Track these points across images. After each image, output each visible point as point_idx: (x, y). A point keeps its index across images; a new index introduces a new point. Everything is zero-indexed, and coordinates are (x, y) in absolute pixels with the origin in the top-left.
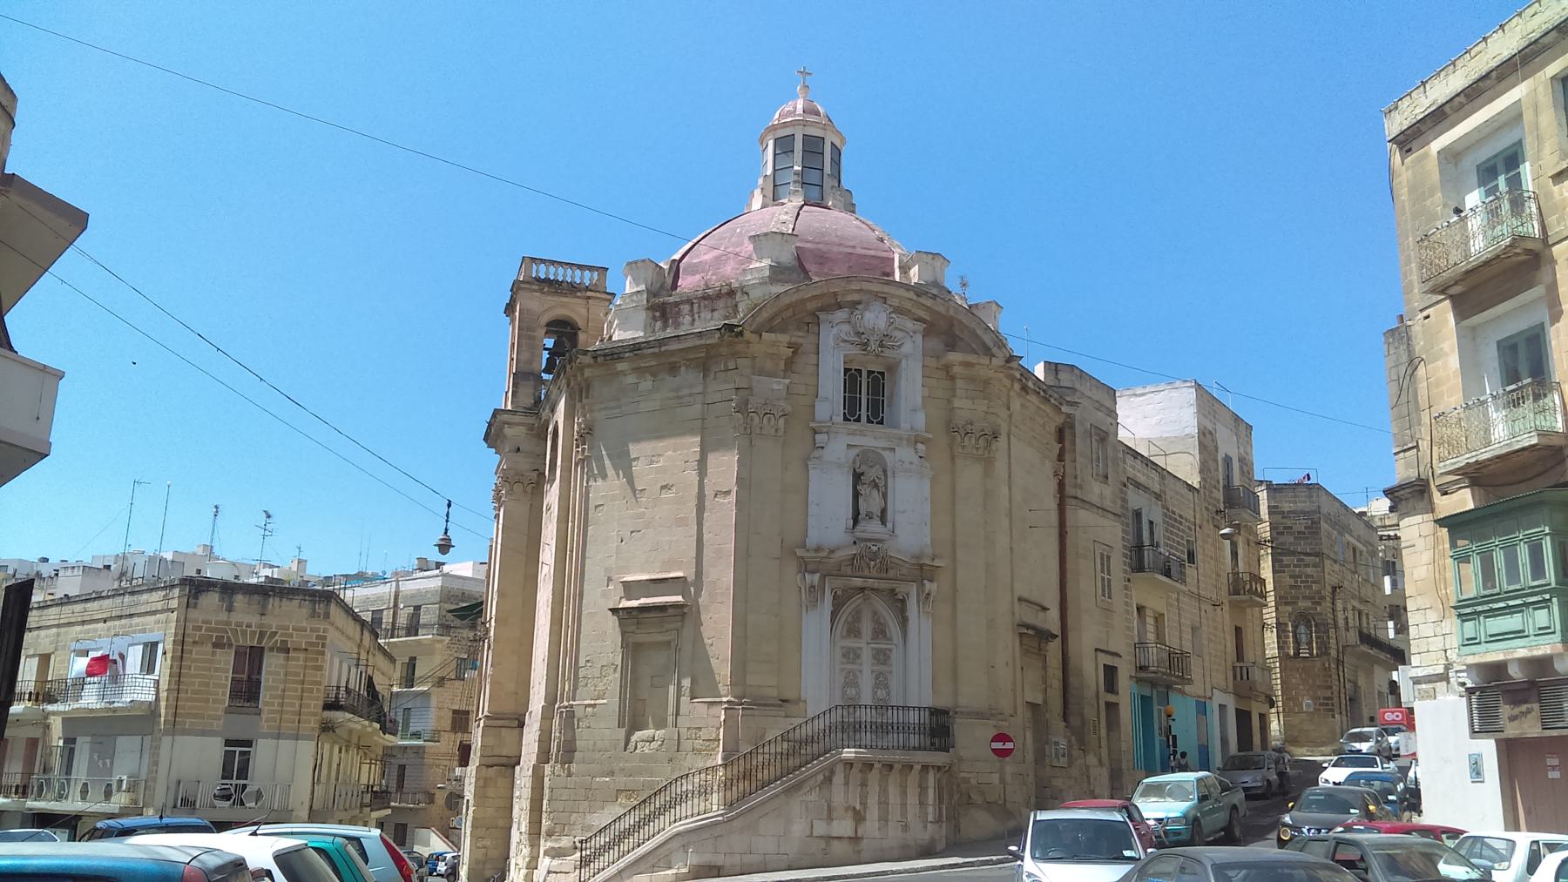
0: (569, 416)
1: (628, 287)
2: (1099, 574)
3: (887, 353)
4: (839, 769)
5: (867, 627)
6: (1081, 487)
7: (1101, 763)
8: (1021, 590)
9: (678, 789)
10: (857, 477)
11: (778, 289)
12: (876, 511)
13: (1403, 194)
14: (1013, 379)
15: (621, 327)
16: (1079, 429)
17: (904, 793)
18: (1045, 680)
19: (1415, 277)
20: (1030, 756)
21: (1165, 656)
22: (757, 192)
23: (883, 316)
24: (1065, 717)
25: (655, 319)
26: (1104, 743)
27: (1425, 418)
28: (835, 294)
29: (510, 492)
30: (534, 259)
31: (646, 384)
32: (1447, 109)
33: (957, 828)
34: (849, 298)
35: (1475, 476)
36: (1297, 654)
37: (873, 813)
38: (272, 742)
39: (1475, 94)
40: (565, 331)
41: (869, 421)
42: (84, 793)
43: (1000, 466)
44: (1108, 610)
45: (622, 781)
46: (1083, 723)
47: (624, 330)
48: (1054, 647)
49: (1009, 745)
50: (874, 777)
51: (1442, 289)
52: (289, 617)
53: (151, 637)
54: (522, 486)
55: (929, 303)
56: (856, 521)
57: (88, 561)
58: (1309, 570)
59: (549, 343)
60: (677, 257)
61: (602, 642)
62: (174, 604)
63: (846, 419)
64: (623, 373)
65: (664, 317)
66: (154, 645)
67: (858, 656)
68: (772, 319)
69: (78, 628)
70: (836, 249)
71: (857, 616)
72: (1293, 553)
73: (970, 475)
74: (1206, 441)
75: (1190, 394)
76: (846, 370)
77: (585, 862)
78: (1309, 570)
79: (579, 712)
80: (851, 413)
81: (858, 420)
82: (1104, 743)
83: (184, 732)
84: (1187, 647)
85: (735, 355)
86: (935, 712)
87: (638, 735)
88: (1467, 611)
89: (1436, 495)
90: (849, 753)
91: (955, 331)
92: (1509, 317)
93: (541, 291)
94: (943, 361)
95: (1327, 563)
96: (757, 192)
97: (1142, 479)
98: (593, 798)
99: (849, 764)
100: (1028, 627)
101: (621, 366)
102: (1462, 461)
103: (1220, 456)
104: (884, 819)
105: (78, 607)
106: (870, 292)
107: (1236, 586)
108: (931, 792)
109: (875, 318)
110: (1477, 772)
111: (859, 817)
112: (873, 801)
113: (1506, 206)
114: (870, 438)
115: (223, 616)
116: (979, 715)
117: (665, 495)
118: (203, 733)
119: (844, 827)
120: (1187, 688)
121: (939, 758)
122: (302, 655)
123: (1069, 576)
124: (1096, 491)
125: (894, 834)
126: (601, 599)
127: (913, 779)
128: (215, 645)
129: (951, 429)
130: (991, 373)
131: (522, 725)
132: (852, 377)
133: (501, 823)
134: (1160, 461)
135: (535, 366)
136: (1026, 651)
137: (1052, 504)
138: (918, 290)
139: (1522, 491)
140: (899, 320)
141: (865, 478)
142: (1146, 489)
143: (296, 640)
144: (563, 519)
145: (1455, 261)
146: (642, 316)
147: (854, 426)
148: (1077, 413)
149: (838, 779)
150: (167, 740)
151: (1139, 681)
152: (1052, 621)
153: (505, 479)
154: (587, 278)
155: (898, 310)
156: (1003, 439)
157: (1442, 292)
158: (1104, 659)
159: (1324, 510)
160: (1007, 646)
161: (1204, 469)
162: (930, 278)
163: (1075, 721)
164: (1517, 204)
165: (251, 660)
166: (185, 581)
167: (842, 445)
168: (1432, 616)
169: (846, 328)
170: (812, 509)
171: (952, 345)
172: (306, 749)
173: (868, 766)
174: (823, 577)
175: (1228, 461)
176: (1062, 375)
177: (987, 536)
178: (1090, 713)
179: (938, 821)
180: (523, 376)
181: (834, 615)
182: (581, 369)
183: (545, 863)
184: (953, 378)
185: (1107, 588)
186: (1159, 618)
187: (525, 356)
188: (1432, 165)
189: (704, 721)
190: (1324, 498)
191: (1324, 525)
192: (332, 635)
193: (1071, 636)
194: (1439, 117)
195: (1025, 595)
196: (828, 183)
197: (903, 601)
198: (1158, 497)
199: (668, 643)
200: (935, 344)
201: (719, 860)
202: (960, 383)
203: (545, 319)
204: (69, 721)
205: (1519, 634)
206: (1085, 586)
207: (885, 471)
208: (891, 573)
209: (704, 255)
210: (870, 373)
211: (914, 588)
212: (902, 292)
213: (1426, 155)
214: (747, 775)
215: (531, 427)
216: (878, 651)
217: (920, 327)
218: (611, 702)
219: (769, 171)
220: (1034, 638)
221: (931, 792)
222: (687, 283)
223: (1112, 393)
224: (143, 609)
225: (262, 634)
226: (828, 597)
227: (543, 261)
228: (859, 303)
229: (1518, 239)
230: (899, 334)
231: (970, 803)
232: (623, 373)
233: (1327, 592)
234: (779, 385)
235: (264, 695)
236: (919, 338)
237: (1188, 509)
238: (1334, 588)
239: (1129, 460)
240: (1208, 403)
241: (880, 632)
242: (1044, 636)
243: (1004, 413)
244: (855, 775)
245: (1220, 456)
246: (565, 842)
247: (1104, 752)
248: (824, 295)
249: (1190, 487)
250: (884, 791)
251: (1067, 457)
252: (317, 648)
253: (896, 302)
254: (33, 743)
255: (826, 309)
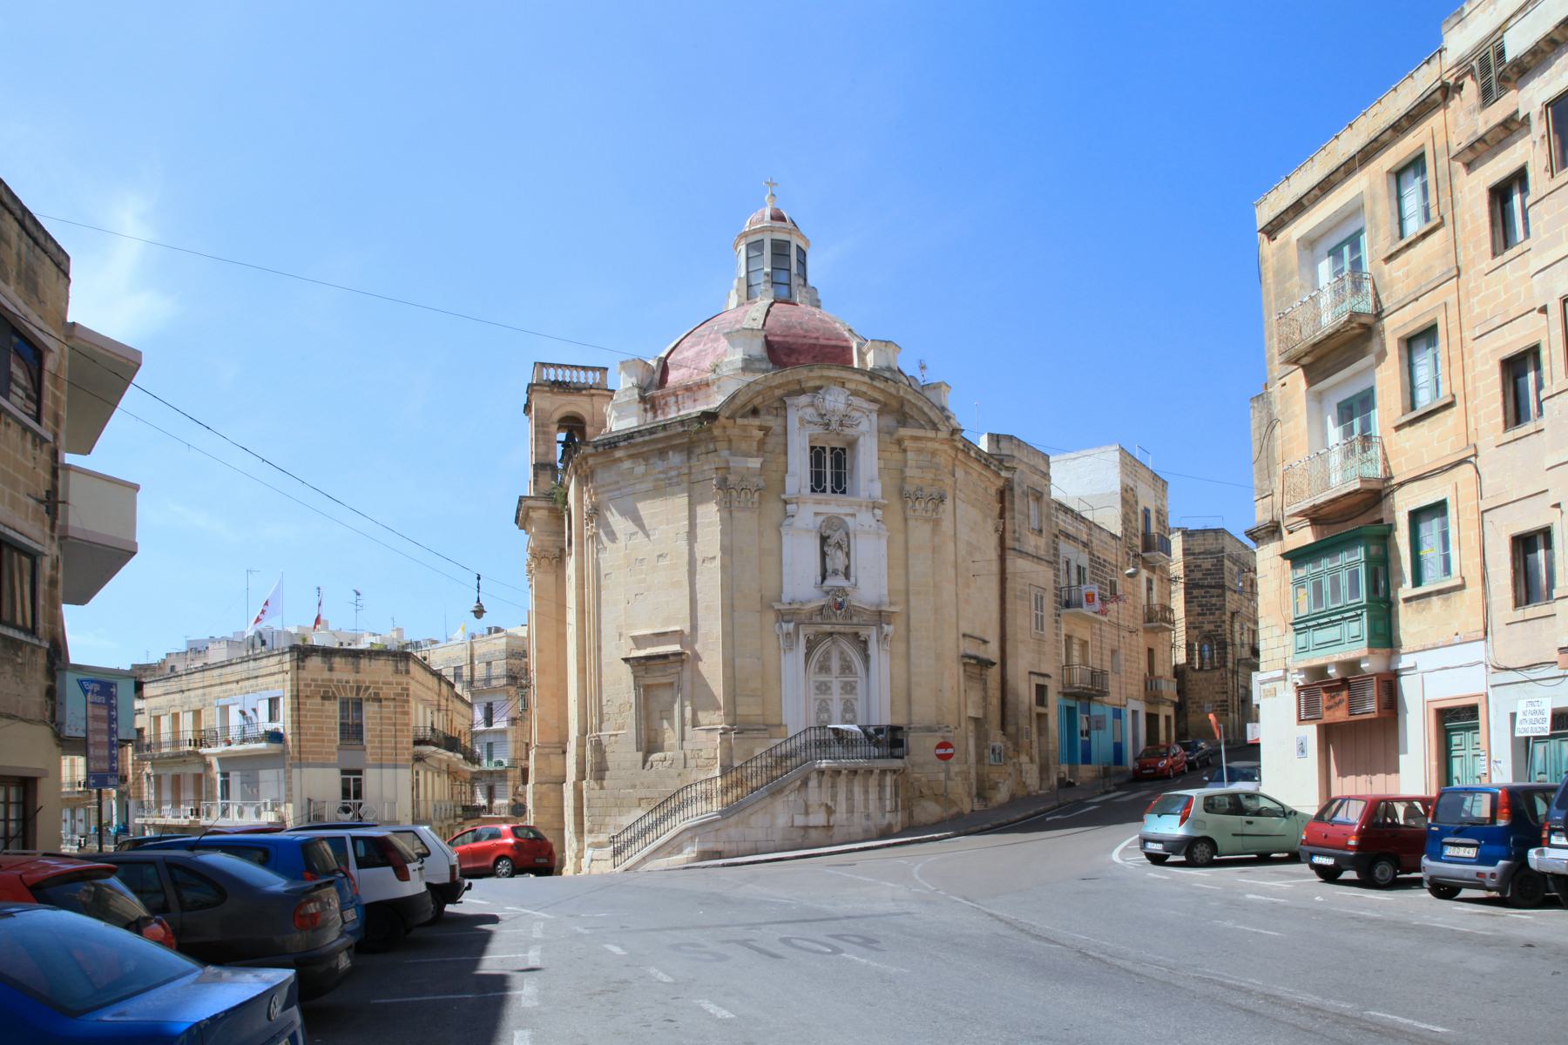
0: (579, 499)
1: (623, 383)
2: (1034, 612)
3: (847, 431)
4: (814, 776)
5: (835, 664)
6: (1018, 540)
7: (1032, 761)
8: (965, 627)
9: (683, 796)
10: (824, 540)
11: (750, 378)
12: (841, 568)
13: (1269, 277)
14: (957, 449)
15: (618, 419)
16: (1017, 491)
17: (866, 792)
18: (985, 698)
19: (1275, 351)
20: (972, 758)
21: (1088, 675)
22: (733, 293)
23: (842, 399)
24: (1003, 726)
25: (645, 410)
26: (1035, 744)
27: (1280, 470)
28: (799, 382)
29: (539, 565)
30: (543, 365)
31: (640, 469)
32: (1305, 201)
33: (911, 815)
34: (811, 384)
35: (1316, 516)
36: (1201, 668)
37: (842, 807)
38: (377, 771)
39: (1326, 186)
40: (574, 426)
41: (833, 491)
42: (241, 813)
43: (947, 525)
44: (1040, 641)
45: (643, 793)
46: (1018, 730)
47: (620, 419)
48: (993, 674)
49: (950, 751)
50: (842, 781)
51: (1294, 360)
52: (378, 673)
53: (273, 694)
54: (550, 558)
55: (881, 385)
56: (824, 578)
57: (230, 635)
58: (1214, 600)
59: (562, 436)
60: (663, 355)
61: (620, 685)
62: (287, 666)
63: (813, 490)
64: (620, 460)
65: (654, 409)
66: (277, 699)
67: (829, 688)
68: (744, 406)
69: (218, 689)
70: (800, 341)
71: (827, 655)
72: (1202, 587)
73: (920, 533)
74: (1128, 497)
75: (1116, 456)
76: (812, 448)
77: (617, 852)
78: (1214, 600)
79: (605, 741)
80: (817, 484)
81: (824, 491)
82: (1035, 744)
83: (309, 765)
84: (1107, 666)
85: (714, 439)
86: (894, 729)
87: (655, 757)
88: (1301, 625)
89: (1285, 532)
90: (824, 764)
91: (906, 407)
92: (1344, 384)
93: (552, 391)
94: (896, 436)
95: (1228, 594)
96: (733, 293)
97: (1071, 530)
98: (621, 805)
99: (821, 772)
100: (970, 657)
101: (619, 454)
102: (1306, 504)
103: (1140, 509)
104: (851, 811)
105: (216, 672)
106: (828, 378)
107: (1150, 616)
108: (888, 790)
109: (835, 400)
110: (1302, 750)
111: (830, 811)
112: (842, 797)
113: (1348, 285)
114: (833, 505)
115: (326, 675)
116: (929, 729)
117: (663, 563)
118: (324, 766)
119: (818, 818)
120: (1106, 699)
121: (897, 764)
122: (392, 704)
123: (1008, 615)
124: (1032, 543)
125: (859, 823)
126: (616, 651)
127: (873, 781)
128: (324, 698)
129: (903, 495)
130: (937, 445)
131: (564, 752)
132: (817, 454)
133: (556, 825)
134: (1088, 515)
135: (551, 457)
136: (969, 677)
137: (993, 554)
138: (873, 375)
139: (1350, 526)
140: (856, 401)
141: (830, 541)
142: (1075, 539)
143: (386, 692)
144: (581, 586)
145: (1309, 335)
146: (637, 408)
147: (819, 496)
148: (1016, 478)
149: (813, 783)
150: (296, 771)
151: (1065, 695)
152: (992, 652)
153: (534, 556)
154: (591, 378)
155: (855, 393)
156: (948, 502)
157: (1295, 363)
158: (1036, 680)
159: (1227, 551)
160: (953, 674)
161: (1126, 520)
162: (884, 364)
163: (1011, 729)
164: (1357, 286)
165: (353, 705)
166: (293, 648)
167: (810, 512)
168: (1277, 632)
169: (810, 410)
170: (786, 569)
171: (903, 419)
172: (405, 775)
173: (838, 772)
174: (797, 625)
175: (1146, 511)
176: (1002, 444)
177: (931, 589)
178: (1024, 723)
179: (894, 810)
180: (541, 467)
181: (808, 656)
182: (585, 458)
183: (588, 853)
184: (905, 451)
185: (1040, 624)
186: (1084, 644)
187: (542, 449)
188: (1292, 252)
189: (700, 742)
190: (1227, 539)
191: (1227, 563)
192: (413, 687)
193: (1009, 662)
194: (1298, 208)
195: (968, 632)
196: (796, 281)
197: (865, 642)
198: (1085, 545)
199: (672, 684)
200: (889, 421)
201: (720, 847)
202: (910, 455)
203: (557, 416)
204: (223, 760)
205: (1337, 642)
206: (1021, 621)
207: (847, 534)
208: (855, 620)
209: (687, 353)
210: (833, 449)
211: (873, 632)
212: (858, 377)
213: (1287, 243)
214: (739, 783)
215: (551, 510)
216: (846, 683)
217: (875, 407)
218: (630, 732)
219: (743, 274)
220: (976, 666)
221: (888, 790)
222: (674, 377)
223: (1046, 458)
224: (263, 672)
225: (359, 688)
226: (802, 641)
227: (552, 365)
228: (820, 388)
229: (1354, 315)
230: (856, 414)
231: (922, 796)
232: (620, 460)
233: (1227, 617)
234: (755, 463)
235: (366, 735)
236: (874, 417)
237: (1112, 554)
238: (1233, 614)
239: (1061, 516)
240: (1130, 463)
241: (847, 668)
242: (985, 664)
243: (949, 481)
244: (826, 779)
245: (1140, 509)
246: (603, 838)
247: (1035, 752)
248: (789, 383)
249: (1114, 536)
250: (850, 793)
251: (1007, 515)
252: (403, 698)
253: (852, 386)
254: (198, 777)
255: (791, 394)
